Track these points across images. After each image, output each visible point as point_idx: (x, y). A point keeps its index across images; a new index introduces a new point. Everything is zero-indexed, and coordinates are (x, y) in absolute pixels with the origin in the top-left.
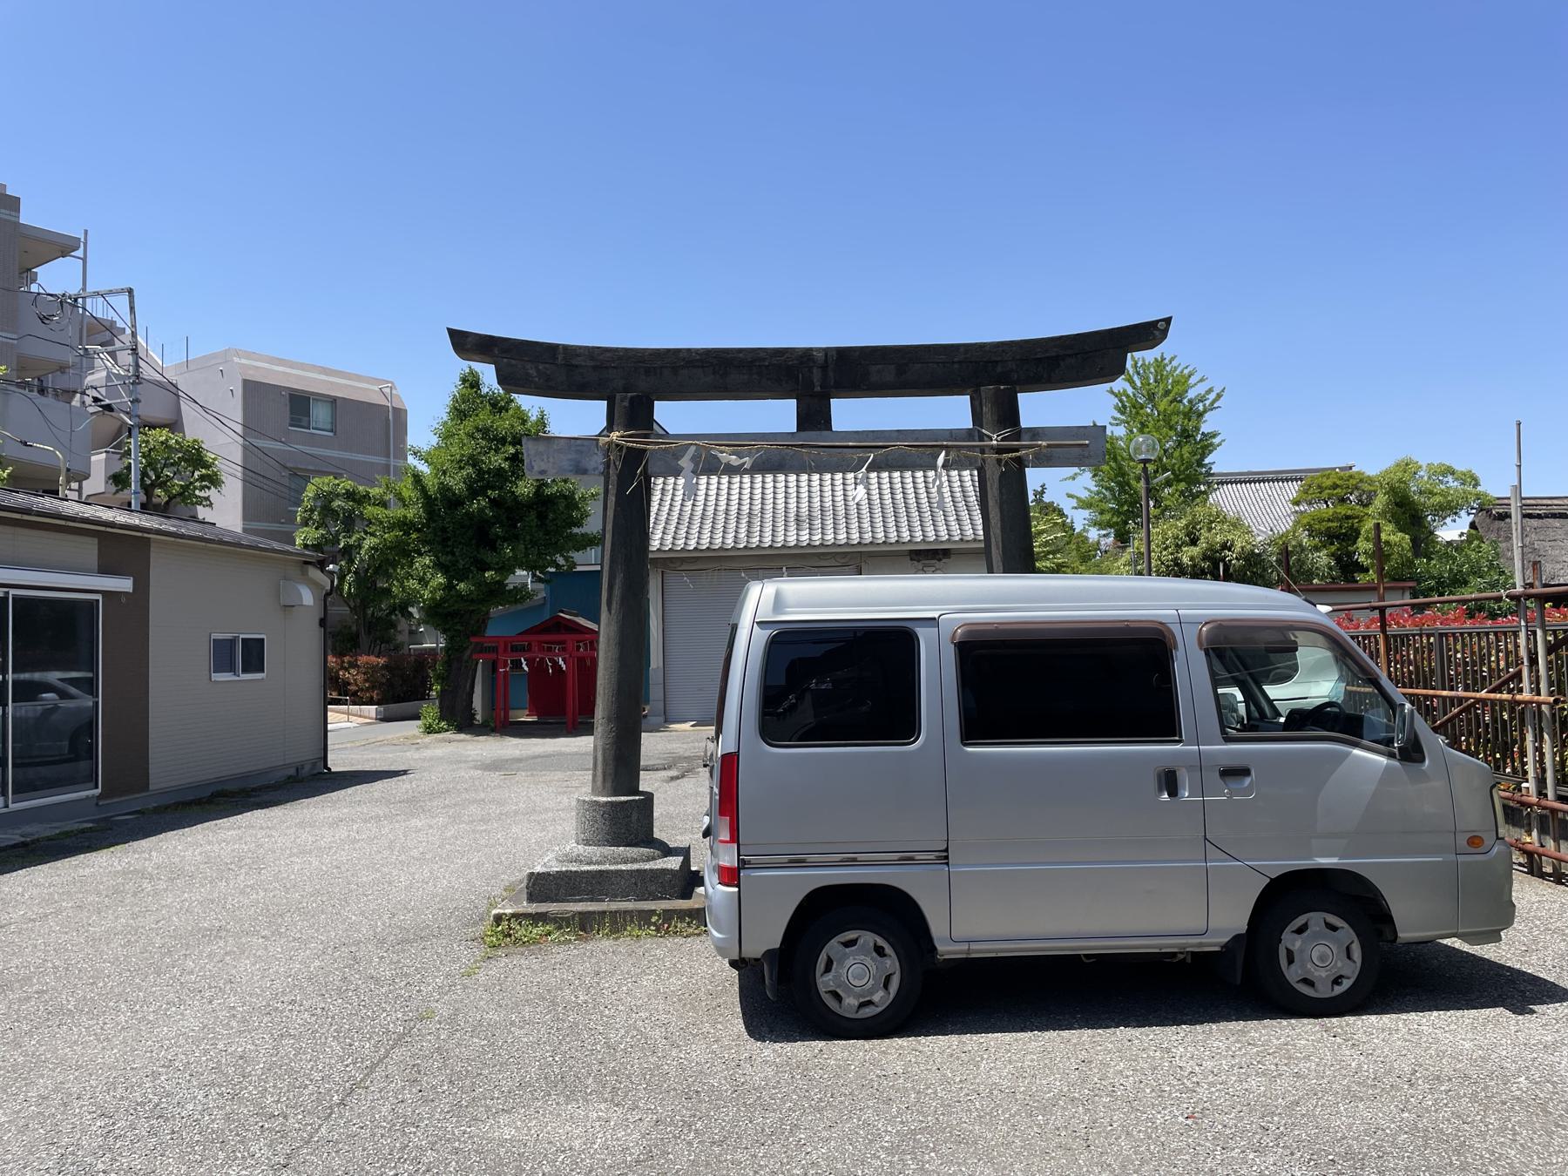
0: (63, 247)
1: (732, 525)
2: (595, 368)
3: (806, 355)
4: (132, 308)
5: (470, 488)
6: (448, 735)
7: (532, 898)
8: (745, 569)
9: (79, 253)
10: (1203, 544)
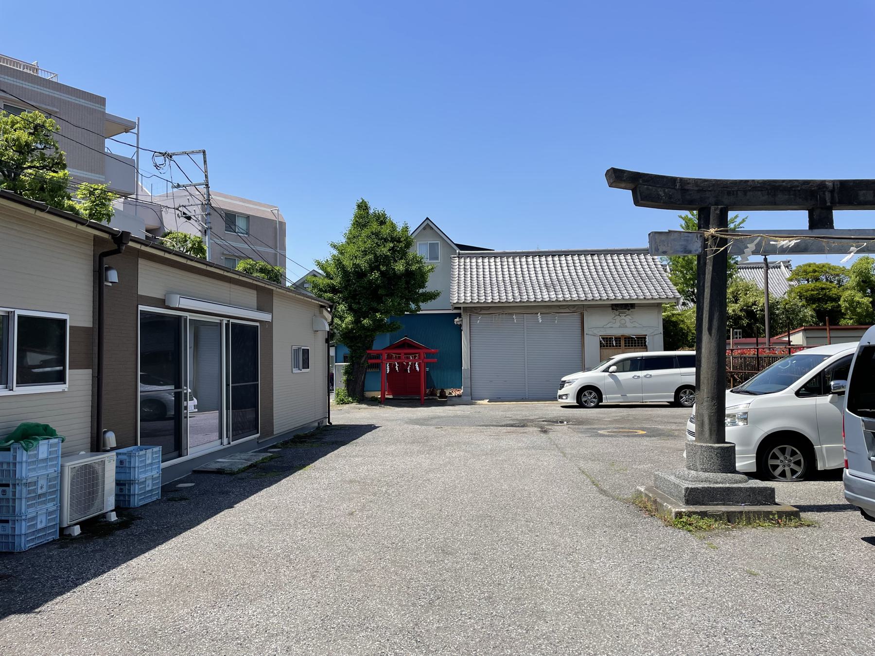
0: (127, 127)
1: (509, 289)
2: (699, 191)
3: (822, 185)
4: (205, 162)
5: (370, 266)
6: (354, 405)
7: (688, 502)
8: (516, 314)
9: (135, 131)
10: (741, 302)
